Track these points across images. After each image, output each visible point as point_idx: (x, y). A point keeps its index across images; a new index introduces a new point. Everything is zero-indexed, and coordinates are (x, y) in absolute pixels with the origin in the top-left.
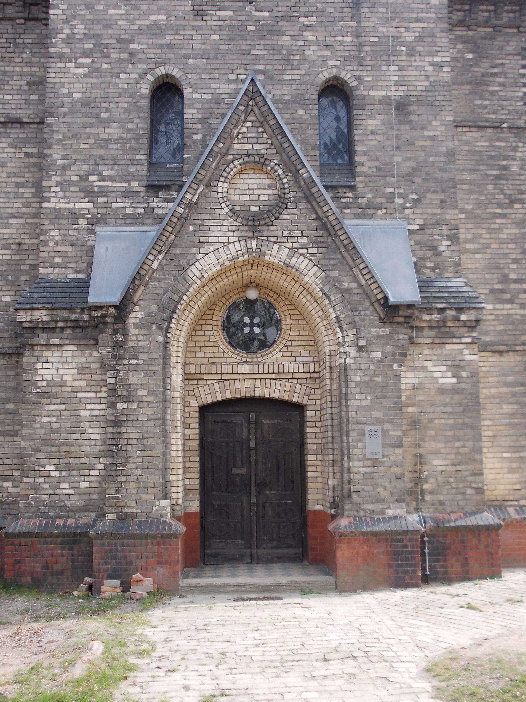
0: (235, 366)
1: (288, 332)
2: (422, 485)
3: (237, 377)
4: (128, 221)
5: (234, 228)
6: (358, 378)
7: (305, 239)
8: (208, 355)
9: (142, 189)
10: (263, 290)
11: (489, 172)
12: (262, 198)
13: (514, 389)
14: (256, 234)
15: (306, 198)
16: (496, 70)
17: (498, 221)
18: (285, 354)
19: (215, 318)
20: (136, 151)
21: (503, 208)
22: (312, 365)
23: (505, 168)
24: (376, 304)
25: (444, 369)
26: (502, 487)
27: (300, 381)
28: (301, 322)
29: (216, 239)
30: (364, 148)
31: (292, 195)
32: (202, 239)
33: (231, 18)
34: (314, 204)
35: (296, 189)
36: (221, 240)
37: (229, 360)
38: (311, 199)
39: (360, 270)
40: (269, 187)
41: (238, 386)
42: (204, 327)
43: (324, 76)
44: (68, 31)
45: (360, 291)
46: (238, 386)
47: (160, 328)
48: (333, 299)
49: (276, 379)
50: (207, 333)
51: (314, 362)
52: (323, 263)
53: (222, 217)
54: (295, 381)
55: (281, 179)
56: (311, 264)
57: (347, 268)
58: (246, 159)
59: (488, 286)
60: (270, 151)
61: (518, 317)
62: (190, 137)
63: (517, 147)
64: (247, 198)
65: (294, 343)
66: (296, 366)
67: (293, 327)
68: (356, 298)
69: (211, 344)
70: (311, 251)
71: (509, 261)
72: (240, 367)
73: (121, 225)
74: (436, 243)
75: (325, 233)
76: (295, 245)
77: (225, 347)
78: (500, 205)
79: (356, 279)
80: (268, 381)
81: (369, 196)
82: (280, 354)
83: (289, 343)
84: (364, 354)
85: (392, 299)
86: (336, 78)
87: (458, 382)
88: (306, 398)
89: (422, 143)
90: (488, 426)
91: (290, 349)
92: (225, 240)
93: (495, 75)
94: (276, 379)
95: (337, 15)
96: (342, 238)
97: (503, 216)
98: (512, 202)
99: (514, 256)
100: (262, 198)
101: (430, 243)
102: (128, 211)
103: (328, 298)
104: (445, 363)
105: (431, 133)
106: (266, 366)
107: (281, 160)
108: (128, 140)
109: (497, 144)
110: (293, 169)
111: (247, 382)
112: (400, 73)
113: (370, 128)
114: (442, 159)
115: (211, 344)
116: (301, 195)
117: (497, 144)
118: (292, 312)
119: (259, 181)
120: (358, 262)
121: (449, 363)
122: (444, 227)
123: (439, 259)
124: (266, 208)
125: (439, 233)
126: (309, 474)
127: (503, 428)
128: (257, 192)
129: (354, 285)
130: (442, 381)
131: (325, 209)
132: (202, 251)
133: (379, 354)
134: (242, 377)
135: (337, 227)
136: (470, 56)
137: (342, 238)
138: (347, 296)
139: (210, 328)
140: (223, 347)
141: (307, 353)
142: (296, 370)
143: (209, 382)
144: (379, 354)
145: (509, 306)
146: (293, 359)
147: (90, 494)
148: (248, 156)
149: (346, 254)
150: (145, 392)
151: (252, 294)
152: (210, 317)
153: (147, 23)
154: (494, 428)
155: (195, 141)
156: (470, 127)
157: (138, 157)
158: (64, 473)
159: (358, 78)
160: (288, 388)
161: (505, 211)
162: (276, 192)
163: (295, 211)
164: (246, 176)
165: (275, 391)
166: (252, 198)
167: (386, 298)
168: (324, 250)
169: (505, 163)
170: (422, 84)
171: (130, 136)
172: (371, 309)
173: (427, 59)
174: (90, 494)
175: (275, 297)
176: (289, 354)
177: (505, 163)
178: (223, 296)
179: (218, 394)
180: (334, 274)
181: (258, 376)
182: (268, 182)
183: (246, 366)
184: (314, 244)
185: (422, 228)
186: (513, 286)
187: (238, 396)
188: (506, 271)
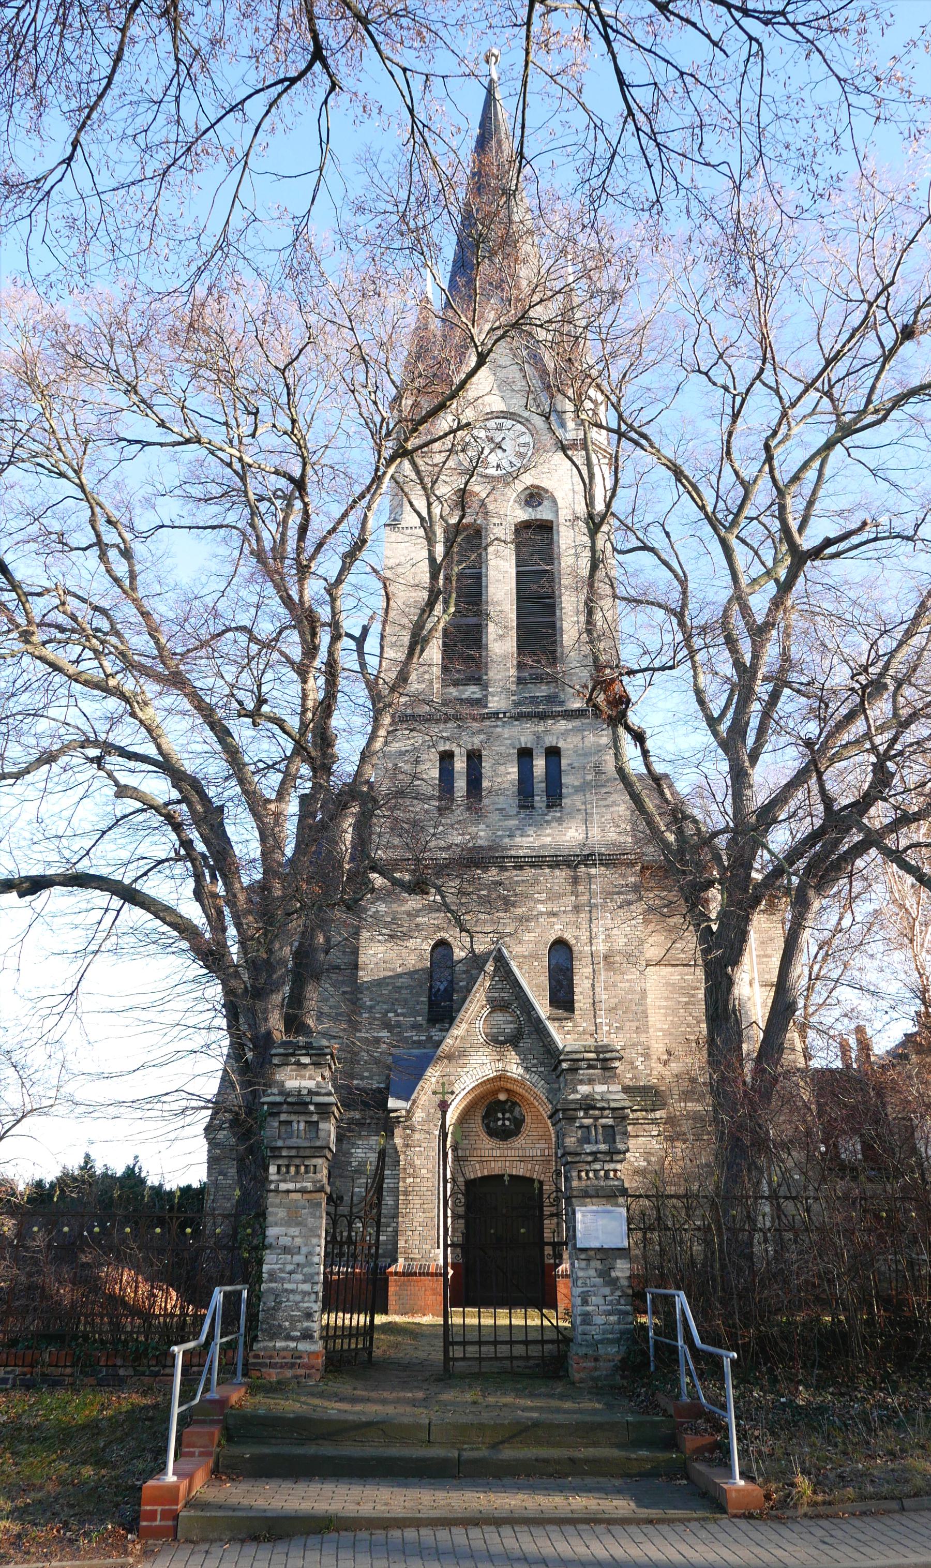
20: (419, 995)
43: (552, 938)
77: (484, 1136)
78: (689, 1026)
151: (502, 1097)
159: (576, 938)
165: (520, 1170)
184: (542, 1064)
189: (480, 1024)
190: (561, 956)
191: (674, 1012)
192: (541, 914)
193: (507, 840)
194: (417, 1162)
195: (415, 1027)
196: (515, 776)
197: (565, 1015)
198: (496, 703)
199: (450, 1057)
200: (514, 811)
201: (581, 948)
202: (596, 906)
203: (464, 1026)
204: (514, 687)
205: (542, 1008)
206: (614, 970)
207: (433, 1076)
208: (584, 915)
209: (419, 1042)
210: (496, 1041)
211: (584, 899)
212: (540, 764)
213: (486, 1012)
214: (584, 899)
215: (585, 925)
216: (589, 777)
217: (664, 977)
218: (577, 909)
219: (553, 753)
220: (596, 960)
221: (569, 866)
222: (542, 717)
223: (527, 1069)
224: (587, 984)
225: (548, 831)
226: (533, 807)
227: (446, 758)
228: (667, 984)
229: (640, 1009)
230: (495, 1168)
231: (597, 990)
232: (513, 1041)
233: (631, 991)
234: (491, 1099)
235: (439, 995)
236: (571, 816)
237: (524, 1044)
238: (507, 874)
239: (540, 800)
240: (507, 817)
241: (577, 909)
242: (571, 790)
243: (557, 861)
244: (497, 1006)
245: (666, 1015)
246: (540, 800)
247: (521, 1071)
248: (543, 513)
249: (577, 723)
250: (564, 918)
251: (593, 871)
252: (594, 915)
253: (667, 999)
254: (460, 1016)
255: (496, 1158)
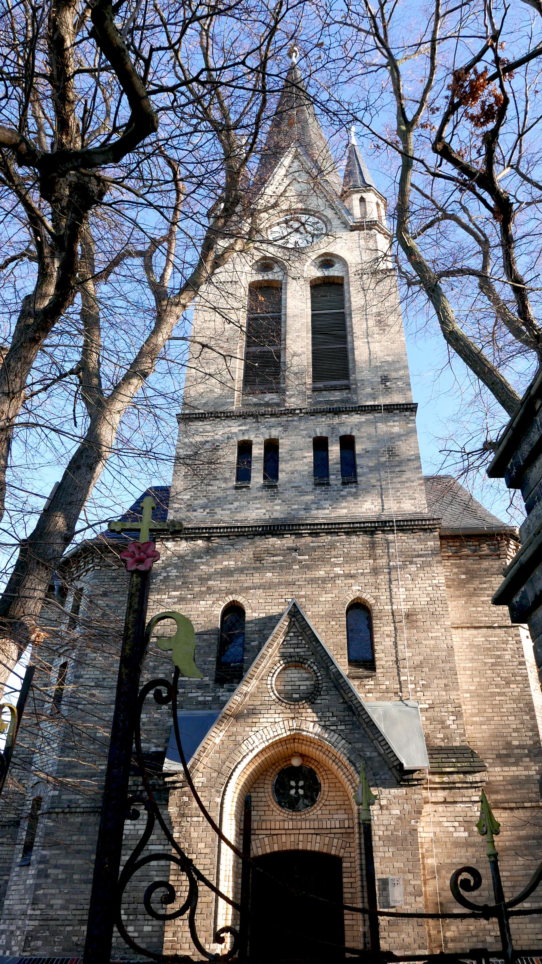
0: (282, 823)
1: (326, 793)
2: (444, 933)
3: (284, 832)
4: (199, 706)
5: (279, 711)
6: (381, 833)
7: (335, 719)
8: (260, 813)
9: (211, 682)
10: (305, 759)
11: (486, 661)
12: (301, 688)
13: (527, 842)
14: (297, 715)
15: (335, 686)
16: (485, 586)
17: (498, 698)
18: (324, 812)
19: (266, 782)
20: (207, 654)
21: (500, 688)
22: (346, 822)
23: (499, 657)
24: (393, 769)
25: (456, 824)
26: (526, 937)
27: (337, 836)
28: (338, 785)
29: (265, 720)
30: (382, 647)
31: (324, 684)
32: (254, 720)
33: (281, 561)
34: (342, 691)
35: (328, 680)
36: (269, 720)
37: (278, 818)
38: (339, 687)
39: (379, 742)
40: (307, 679)
41: (284, 840)
42: (257, 790)
43: (350, 598)
44: (165, 574)
45: (381, 759)
46: (284, 840)
47: (218, 792)
48: (358, 766)
49: (317, 834)
50: (260, 795)
51: (348, 819)
52: (350, 737)
53: (270, 703)
54: (332, 836)
55: (316, 673)
56: (340, 738)
57: (369, 740)
58: (289, 659)
59: (494, 752)
60: (307, 653)
61: (524, 778)
62: (249, 644)
63: (508, 640)
64: (290, 688)
65: (331, 803)
66: (333, 822)
67: (331, 789)
68: (377, 765)
69: (263, 804)
70: (339, 727)
71: (511, 730)
72: (286, 823)
73: (194, 709)
74: (444, 718)
75: (351, 713)
76: (327, 723)
77: (274, 806)
78: (497, 686)
79: (376, 750)
80: (310, 836)
81: (387, 683)
82: (319, 812)
83: (327, 803)
84: (385, 812)
85: (406, 766)
86: (358, 598)
87: (469, 836)
88: (342, 850)
89: (427, 642)
90: (507, 877)
91: (328, 807)
92: (272, 720)
93: (485, 589)
94: (317, 834)
95: (358, 555)
96: (364, 717)
97: (504, 694)
98: (508, 683)
99: (515, 726)
100: (301, 688)
101: (439, 718)
102: (200, 699)
103: (354, 765)
104: (457, 819)
105: (434, 635)
106: (308, 823)
107: (316, 659)
108: (202, 648)
109: (491, 639)
110: (325, 666)
111: (292, 836)
112: (407, 593)
113: (386, 633)
114: (444, 653)
115: (263, 804)
116: (331, 685)
117: (491, 639)
118: (329, 776)
119: (299, 675)
120: (376, 735)
121: (461, 819)
122: (450, 705)
123: (447, 731)
124: (305, 695)
125: (446, 710)
126: (346, 922)
127: (521, 878)
128: (297, 683)
129: (375, 754)
130: (455, 835)
131: (350, 695)
132: (254, 729)
133: (398, 812)
134: (288, 832)
135: (359, 709)
136: (463, 577)
137: (364, 717)
138: (369, 763)
139: (262, 790)
140: (272, 806)
141: (343, 812)
142: (333, 826)
143: (260, 837)
144: (398, 812)
145: (515, 768)
146: (330, 816)
147: (151, 937)
148: (291, 657)
149: (367, 729)
150: (203, 845)
151: (296, 762)
152: (262, 781)
153: (221, 567)
154: (512, 879)
155: (253, 647)
156: (468, 627)
157: (210, 659)
158: (131, 917)
159: (376, 598)
160: (326, 842)
161: (503, 690)
162: (312, 683)
163: (327, 697)
164: (290, 672)
165: (315, 845)
166: (294, 687)
167: (401, 765)
168: (350, 727)
169: (499, 653)
170: (424, 600)
171: (204, 644)
172: (390, 773)
173: (427, 582)
174: (151, 937)
175: (316, 764)
176: (327, 812)
177: (499, 653)
178: (274, 764)
179: (268, 847)
180: (359, 745)
181: (301, 831)
182: (306, 675)
183: (291, 823)
184: (343, 722)
185: (431, 707)
186: (516, 751)
187: (284, 849)
188: (509, 739)
189: (272, 681)
190: (360, 614)
191: (481, 673)
192: (338, 576)
193: (302, 512)
194: (194, 835)
195: (201, 686)
196: (311, 459)
197: (366, 673)
198: (292, 402)
199: (238, 717)
200: (310, 488)
201: (380, 605)
202: (395, 568)
203: (254, 682)
204: (309, 393)
205: (342, 665)
206: (417, 627)
207: (216, 737)
208: (383, 578)
209: (204, 703)
210: (290, 699)
211: (383, 562)
212: (334, 451)
213: (279, 667)
214: (383, 562)
215: (384, 586)
216: (383, 459)
217: (466, 639)
218: (375, 571)
219: (348, 443)
220: (397, 619)
221: (365, 532)
222: (337, 412)
223: (325, 727)
224: (389, 642)
225: (344, 504)
226: (328, 484)
227: (245, 448)
228: (471, 646)
229: (448, 665)
230: (287, 843)
231: (400, 647)
232: (311, 698)
233: (435, 648)
234: (283, 765)
235: (232, 645)
236: (367, 491)
237: (322, 700)
238: (303, 540)
239: (335, 479)
240: (304, 493)
241: (375, 571)
242: (365, 470)
243: (354, 528)
244: (291, 661)
245: (472, 676)
246: (335, 479)
247: (318, 729)
248: (335, 272)
249: (370, 416)
250: (362, 579)
251: (391, 537)
252: (393, 577)
253: (472, 660)
254: (250, 671)
255: (285, 831)
